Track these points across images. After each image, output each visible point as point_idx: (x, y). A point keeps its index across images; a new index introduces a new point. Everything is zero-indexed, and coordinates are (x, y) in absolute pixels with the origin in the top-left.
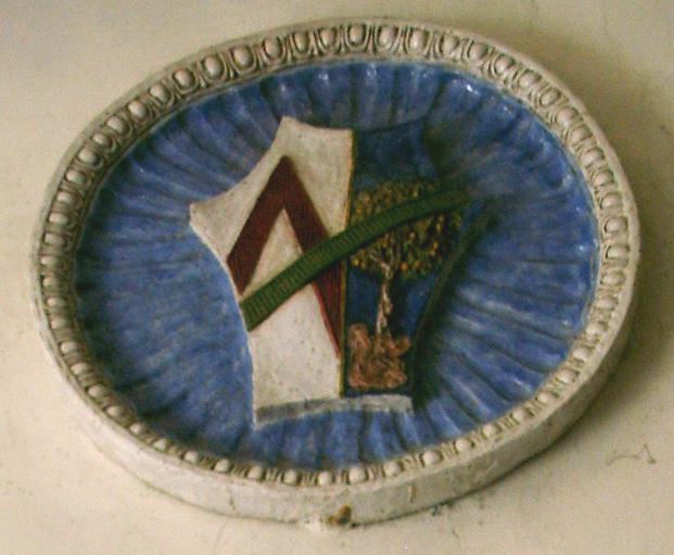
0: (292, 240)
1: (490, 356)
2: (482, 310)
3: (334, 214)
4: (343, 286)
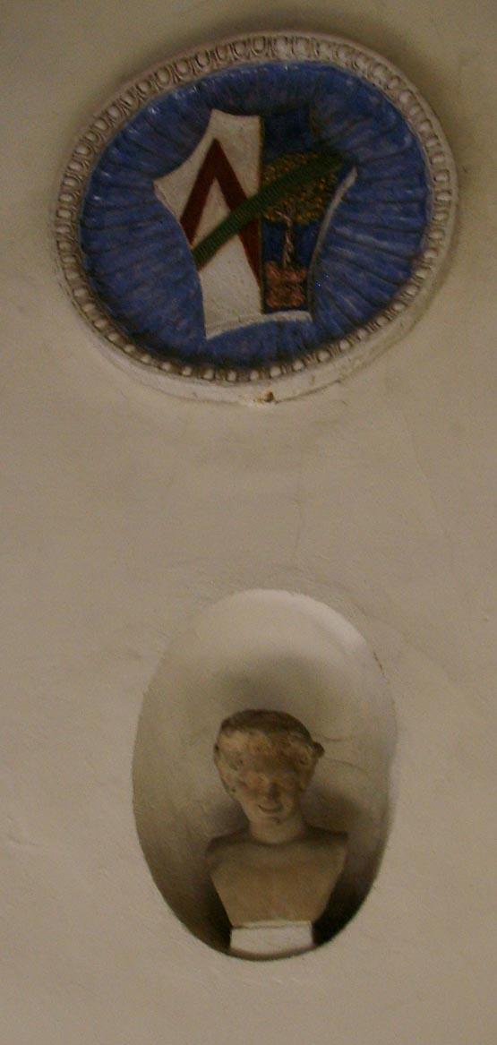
0: (223, 202)
1: (361, 275)
2: (353, 241)
3: (249, 179)
4: (260, 234)
